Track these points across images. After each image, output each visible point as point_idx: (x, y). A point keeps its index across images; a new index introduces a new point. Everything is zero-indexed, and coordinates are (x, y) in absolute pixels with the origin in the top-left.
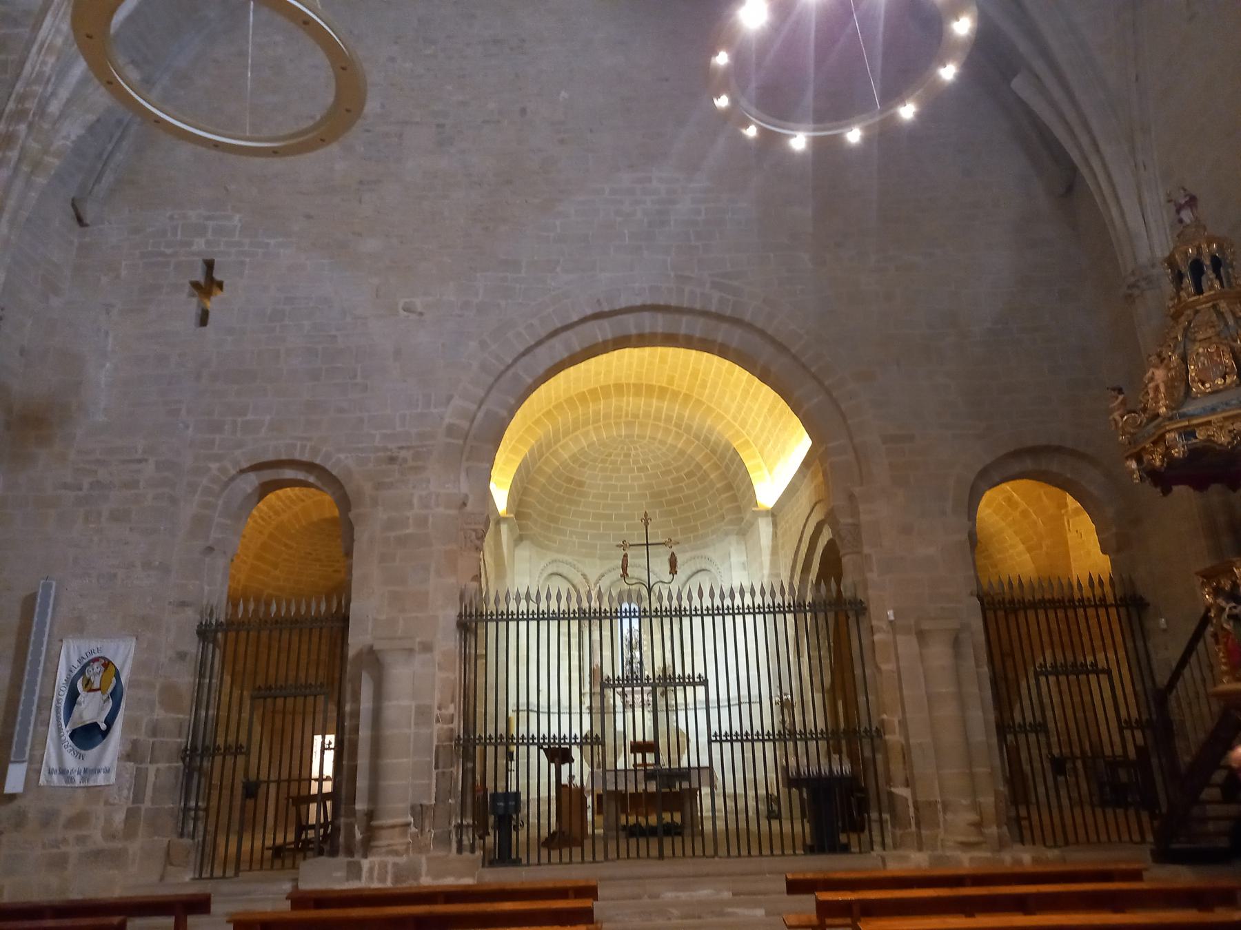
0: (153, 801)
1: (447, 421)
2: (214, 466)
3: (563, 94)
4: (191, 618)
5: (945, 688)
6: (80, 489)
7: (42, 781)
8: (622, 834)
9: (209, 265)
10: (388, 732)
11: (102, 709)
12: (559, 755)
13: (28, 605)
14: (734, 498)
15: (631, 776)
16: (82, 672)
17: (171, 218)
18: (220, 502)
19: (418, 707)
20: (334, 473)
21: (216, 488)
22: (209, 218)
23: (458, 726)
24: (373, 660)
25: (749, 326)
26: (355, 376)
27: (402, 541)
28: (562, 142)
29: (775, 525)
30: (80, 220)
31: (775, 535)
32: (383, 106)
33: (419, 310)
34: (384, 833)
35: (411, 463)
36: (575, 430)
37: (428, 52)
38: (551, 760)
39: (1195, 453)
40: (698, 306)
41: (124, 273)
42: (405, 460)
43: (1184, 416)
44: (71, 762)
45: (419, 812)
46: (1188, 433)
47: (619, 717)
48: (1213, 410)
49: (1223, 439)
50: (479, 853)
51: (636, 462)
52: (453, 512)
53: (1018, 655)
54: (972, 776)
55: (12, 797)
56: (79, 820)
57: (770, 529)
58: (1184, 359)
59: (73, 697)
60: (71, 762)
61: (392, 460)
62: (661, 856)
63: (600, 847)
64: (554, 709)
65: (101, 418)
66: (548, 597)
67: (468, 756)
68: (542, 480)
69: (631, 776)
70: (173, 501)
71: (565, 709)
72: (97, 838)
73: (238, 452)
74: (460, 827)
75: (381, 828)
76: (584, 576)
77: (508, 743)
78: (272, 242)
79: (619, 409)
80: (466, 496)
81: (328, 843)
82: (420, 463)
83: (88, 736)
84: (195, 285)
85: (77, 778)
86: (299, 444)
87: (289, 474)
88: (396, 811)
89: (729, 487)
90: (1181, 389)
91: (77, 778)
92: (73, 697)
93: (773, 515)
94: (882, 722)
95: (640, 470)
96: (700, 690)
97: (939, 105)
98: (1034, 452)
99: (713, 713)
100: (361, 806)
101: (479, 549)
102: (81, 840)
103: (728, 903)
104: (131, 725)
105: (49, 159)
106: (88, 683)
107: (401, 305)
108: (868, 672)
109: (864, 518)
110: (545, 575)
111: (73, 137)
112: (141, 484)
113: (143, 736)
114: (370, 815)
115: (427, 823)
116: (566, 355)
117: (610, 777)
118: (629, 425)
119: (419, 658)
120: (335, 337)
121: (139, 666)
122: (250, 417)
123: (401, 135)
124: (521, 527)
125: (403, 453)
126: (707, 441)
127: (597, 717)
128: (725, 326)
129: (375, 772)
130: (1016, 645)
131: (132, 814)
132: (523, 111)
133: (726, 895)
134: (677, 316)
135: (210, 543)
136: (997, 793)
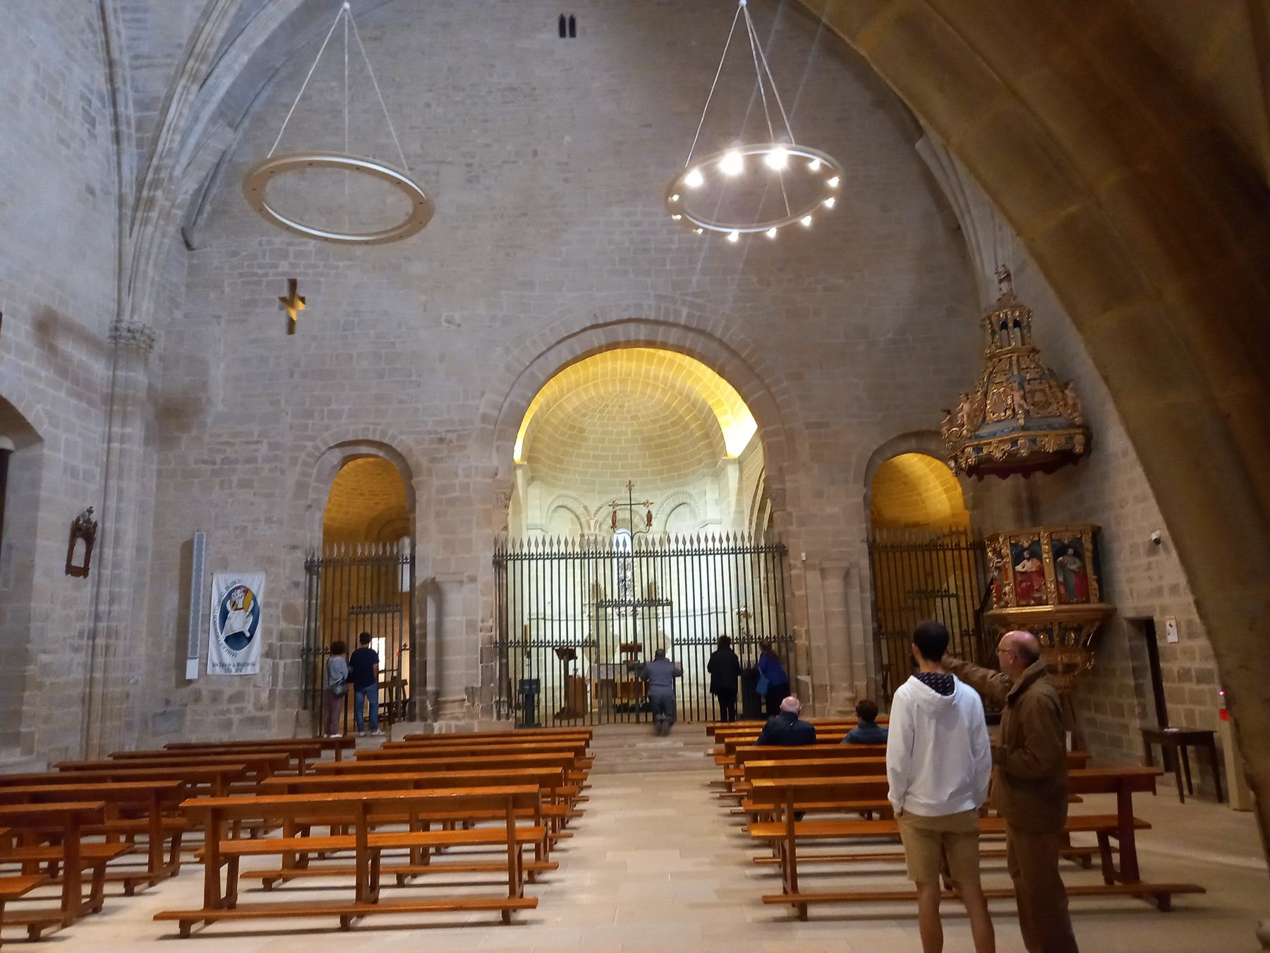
0: (284, 685)
1: (482, 410)
2: (309, 444)
3: (567, 138)
4: (300, 557)
5: (837, 609)
6: (214, 463)
7: (209, 671)
8: (611, 710)
9: (293, 284)
10: (448, 638)
11: (246, 622)
12: (566, 653)
13: (187, 549)
14: (710, 445)
15: (617, 668)
16: (229, 596)
17: (260, 244)
18: (315, 471)
19: (468, 621)
20: (399, 450)
21: (311, 460)
22: (290, 244)
23: (495, 634)
24: (435, 588)
25: (710, 336)
26: (411, 375)
27: (452, 502)
28: (566, 180)
29: (741, 471)
30: (188, 245)
31: (741, 478)
32: (422, 147)
33: (458, 321)
34: (448, 705)
35: (455, 443)
36: (577, 386)
37: (457, 99)
38: (560, 658)
39: (980, 462)
40: (671, 320)
41: (227, 290)
42: (451, 441)
43: (977, 437)
44: (228, 659)
45: (471, 692)
46: (978, 449)
47: (616, 623)
48: (994, 435)
49: (998, 455)
50: (512, 720)
51: (629, 412)
52: (490, 480)
53: (936, 576)
54: (851, 668)
55: (190, 682)
56: (237, 697)
57: (737, 475)
58: (985, 395)
59: (224, 615)
60: (228, 659)
61: (441, 440)
62: (638, 722)
63: (595, 719)
64: (563, 617)
65: (220, 408)
66: (559, 543)
67: (503, 654)
68: (550, 430)
69: (617, 668)
70: (283, 472)
71: (571, 617)
72: (250, 709)
73: (326, 434)
74: (498, 702)
75: (445, 702)
76: (585, 508)
77: (525, 646)
78: (341, 264)
79: (614, 370)
80: (497, 468)
81: (399, 711)
82: (462, 443)
83: (237, 640)
84: (283, 299)
85: (233, 670)
86: (371, 427)
87: (364, 450)
88: (455, 690)
89: (707, 436)
90: (979, 418)
91: (233, 670)
92: (224, 615)
93: (740, 462)
94: (794, 631)
95: (633, 418)
96: (667, 609)
97: (823, 219)
98: (919, 435)
99: (676, 621)
100: (430, 688)
101: (507, 507)
102: (240, 710)
103: (680, 749)
104: (267, 633)
105: (174, 211)
106: (234, 604)
107: (444, 315)
108: (787, 596)
109: (788, 485)
110: (553, 507)
111: (191, 192)
112: (259, 460)
113: (274, 640)
114: (438, 694)
115: (477, 699)
116: (570, 358)
117: (603, 669)
118: (624, 382)
119: (467, 587)
120: (393, 343)
121: (270, 592)
122: (333, 406)
123: (438, 174)
124: (533, 470)
125: (449, 436)
126: (688, 397)
127: (594, 623)
128: (691, 335)
129: (440, 665)
130: (935, 567)
131: (272, 693)
132: (535, 153)
133: (681, 745)
134: (655, 327)
135: (309, 502)
136: (868, 679)
